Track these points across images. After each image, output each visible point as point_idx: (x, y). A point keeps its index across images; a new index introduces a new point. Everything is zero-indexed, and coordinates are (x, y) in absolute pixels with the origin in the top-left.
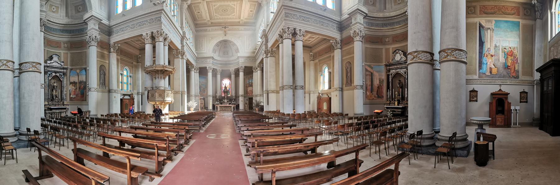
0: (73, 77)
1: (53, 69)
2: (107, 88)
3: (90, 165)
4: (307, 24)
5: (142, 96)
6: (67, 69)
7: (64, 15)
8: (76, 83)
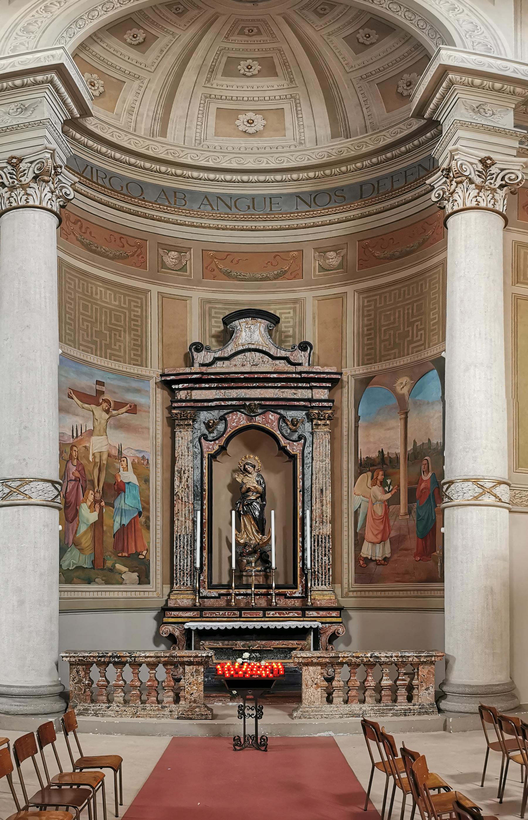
0: (373, 424)
1: (234, 393)
4: (145, 216)
6: (334, 382)
8: (394, 462)
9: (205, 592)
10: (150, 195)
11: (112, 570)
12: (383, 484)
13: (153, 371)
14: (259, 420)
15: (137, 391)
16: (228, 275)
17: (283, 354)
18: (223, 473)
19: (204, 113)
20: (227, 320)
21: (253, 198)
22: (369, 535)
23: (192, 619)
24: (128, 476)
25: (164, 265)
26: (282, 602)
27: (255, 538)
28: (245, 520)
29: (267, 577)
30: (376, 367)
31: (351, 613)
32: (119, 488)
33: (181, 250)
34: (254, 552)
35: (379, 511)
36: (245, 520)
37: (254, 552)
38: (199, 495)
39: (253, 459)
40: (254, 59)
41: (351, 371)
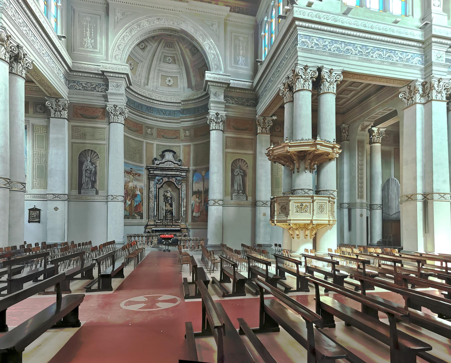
1: (164, 173)
2: (250, 198)
3: (283, 337)
5: (425, 204)
6: (187, 171)
7: (186, 85)
9: (157, 221)
10: (144, 109)
11: (134, 216)
12: (199, 198)
13: (144, 165)
14: (171, 180)
15: (140, 170)
16: (163, 137)
17: (177, 162)
18: (162, 192)
19: (158, 76)
20: (163, 152)
21: (170, 111)
22: (195, 210)
23: (154, 227)
24: (138, 193)
25: (147, 133)
26: (176, 224)
27: (169, 208)
28: (167, 204)
29: (172, 218)
30: (198, 167)
31: (190, 230)
32: (136, 196)
33: (152, 128)
34: (169, 212)
35: (197, 204)
36: (167, 204)
37: (169, 212)
38: (156, 198)
39: (169, 189)
40: (171, 57)
41: (192, 168)
